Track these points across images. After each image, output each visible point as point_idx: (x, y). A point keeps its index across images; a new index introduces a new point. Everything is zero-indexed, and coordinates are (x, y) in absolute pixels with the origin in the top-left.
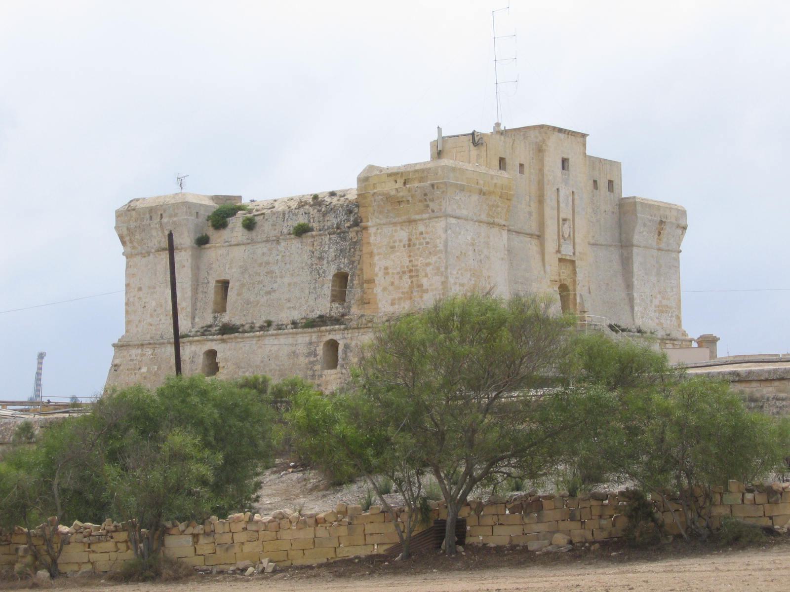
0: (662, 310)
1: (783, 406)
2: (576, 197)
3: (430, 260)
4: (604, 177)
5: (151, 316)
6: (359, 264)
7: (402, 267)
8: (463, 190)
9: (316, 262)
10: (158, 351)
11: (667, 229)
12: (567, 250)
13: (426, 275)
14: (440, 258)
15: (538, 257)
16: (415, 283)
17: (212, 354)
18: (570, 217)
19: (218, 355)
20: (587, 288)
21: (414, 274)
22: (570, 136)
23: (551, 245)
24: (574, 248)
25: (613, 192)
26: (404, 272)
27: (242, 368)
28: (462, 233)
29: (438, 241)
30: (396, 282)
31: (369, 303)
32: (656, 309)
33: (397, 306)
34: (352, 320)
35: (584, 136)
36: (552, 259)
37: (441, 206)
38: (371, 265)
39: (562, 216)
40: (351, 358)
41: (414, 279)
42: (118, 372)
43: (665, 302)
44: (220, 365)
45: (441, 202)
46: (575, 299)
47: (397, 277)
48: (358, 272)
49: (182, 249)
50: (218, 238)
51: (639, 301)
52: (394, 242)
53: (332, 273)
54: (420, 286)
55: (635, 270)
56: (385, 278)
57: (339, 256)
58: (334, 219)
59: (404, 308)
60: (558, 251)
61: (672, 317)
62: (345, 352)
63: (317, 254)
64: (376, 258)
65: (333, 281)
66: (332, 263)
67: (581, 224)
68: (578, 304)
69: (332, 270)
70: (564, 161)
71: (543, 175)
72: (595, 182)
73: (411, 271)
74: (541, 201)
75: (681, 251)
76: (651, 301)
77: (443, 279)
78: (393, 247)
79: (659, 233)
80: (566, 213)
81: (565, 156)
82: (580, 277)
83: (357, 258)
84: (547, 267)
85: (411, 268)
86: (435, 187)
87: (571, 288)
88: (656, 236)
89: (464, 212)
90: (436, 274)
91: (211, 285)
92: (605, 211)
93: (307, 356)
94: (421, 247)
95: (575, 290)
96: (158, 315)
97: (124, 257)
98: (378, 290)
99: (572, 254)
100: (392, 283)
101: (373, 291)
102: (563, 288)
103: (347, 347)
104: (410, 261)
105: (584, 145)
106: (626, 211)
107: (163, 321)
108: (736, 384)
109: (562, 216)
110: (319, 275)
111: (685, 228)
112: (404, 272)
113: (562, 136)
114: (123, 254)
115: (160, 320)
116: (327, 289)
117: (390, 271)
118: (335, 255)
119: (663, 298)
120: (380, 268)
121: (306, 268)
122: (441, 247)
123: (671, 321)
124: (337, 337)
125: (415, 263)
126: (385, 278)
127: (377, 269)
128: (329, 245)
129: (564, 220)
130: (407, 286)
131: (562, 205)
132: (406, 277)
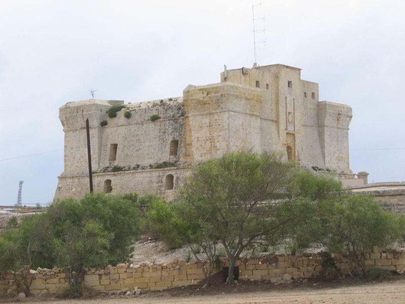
4: (310, 91)
10: (81, 180)
11: (342, 118)
12: (291, 128)
13: (218, 141)
18: (292, 111)
23: (282, 126)
26: (207, 140)
30: (203, 145)
31: (189, 156)
33: (203, 157)
35: (299, 70)
36: (283, 133)
38: (191, 136)
39: (288, 111)
43: (341, 155)
44: (113, 187)
50: (112, 122)
52: (202, 124)
60: (286, 129)
61: (344, 163)
62: (177, 181)
63: (162, 130)
64: (193, 133)
65: (171, 144)
67: (298, 115)
69: (170, 139)
70: (289, 83)
72: (305, 93)
73: (211, 139)
74: (277, 103)
76: (334, 155)
77: (227, 143)
78: (201, 127)
80: (290, 109)
82: (297, 142)
84: (280, 136)
88: (336, 121)
89: (238, 109)
95: (295, 149)
98: (194, 149)
102: (289, 148)
103: (178, 178)
105: (300, 74)
106: (321, 108)
109: (288, 111)
111: (351, 117)
112: (207, 140)
113: (288, 70)
116: (168, 149)
117: (200, 139)
122: (226, 127)
124: (172, 173)
129: (289, 113)
130: (209, 147)
131: (288, 105)
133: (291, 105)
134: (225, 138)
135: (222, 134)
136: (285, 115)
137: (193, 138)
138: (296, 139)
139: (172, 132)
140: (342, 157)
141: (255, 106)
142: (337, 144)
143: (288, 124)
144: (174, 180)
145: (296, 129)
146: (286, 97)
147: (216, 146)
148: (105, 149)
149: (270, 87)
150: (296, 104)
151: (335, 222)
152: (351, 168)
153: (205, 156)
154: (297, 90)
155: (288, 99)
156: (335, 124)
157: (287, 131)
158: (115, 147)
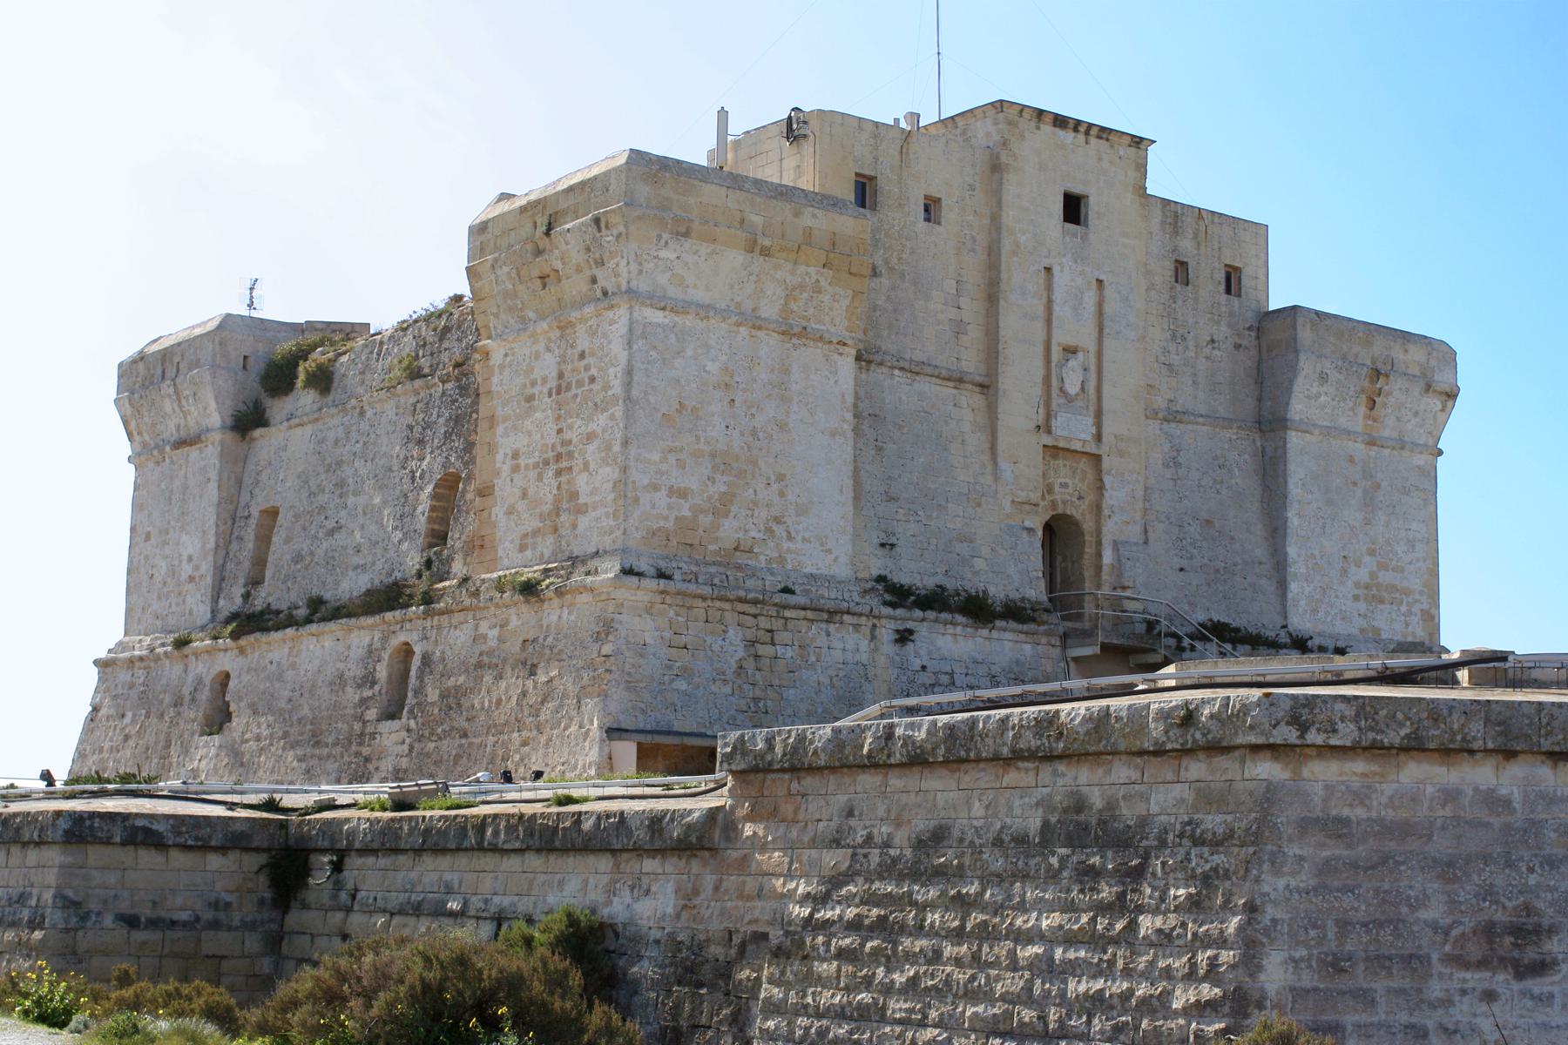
0: (1374, 594)
1: (1215, 869)
2: (1109, 292)
4: (1210, 258)
5: (159, 598)
8: (686, 234)
11: (1395, 389)
12: (1074, 428)
15: (976, 440)
16: (564, 486)
18: (1087, 340)
22: (1093, 140)
24: (1099, 424)
25: (1239, 295)
26: (546, 463)
28: (689, 353)
32: (1356, 592)
35: (1138, 142)
38: (492, 448)
39: (1060, 337)
40: (429, 689)
43: (1386, 577)
46: (1099, 555)
47: (533, 474)
50: (278, 409)
51: (1303, 570)
52: (533, 384)
54: (574, 495)
60: (1045, 427)
61: (1410, 613)
64: (500, 430)
66: (437, 452)
68: (1105, 570)
70: (1073, 208)
71: (999, 229)
73: (559, 457)
74: (992, 296)
75: (1440, 453)
76: (1344, 572)
78: (530, 399)
79: (1372, 404)
80: (1074, 328)
81: (1077, 190)
82: (1115, 495)
84: (1003, 464)
85: (559, 449)
86: (603, 225)
87: (1088, 525)
92: (1213, 341)
95: (1099, 532)
99: (1088, 437)
103: (426, 660)
104: (560, 431)
105: (1142, 168)
106: (1276, 339)
107: (174, 609)
108: (1061, 767)
111: (1451, 395)
112: (546, 463)
113: (1067, 136)
119: (1383, 566)
120: (506, 455)
122: (617, 387)
123: (1407, 625)
125: (568, 435)
129: (1071, 351)
130: (550, 498)
134: (608, 448)
136: (1039, 363)
137: (499, 457)
138: (1107, 479)
140: (1392, 588)
142: (1367, 522)
143: (1057, 400)
144: (413, 673)
145: (1107, 430)
146: (1048, 269)
149: (949, 214)
150: (1109, 309)
154: (1121, 247)
156: (1353, 418)
157: (1049, 441)
158: (272, 514)
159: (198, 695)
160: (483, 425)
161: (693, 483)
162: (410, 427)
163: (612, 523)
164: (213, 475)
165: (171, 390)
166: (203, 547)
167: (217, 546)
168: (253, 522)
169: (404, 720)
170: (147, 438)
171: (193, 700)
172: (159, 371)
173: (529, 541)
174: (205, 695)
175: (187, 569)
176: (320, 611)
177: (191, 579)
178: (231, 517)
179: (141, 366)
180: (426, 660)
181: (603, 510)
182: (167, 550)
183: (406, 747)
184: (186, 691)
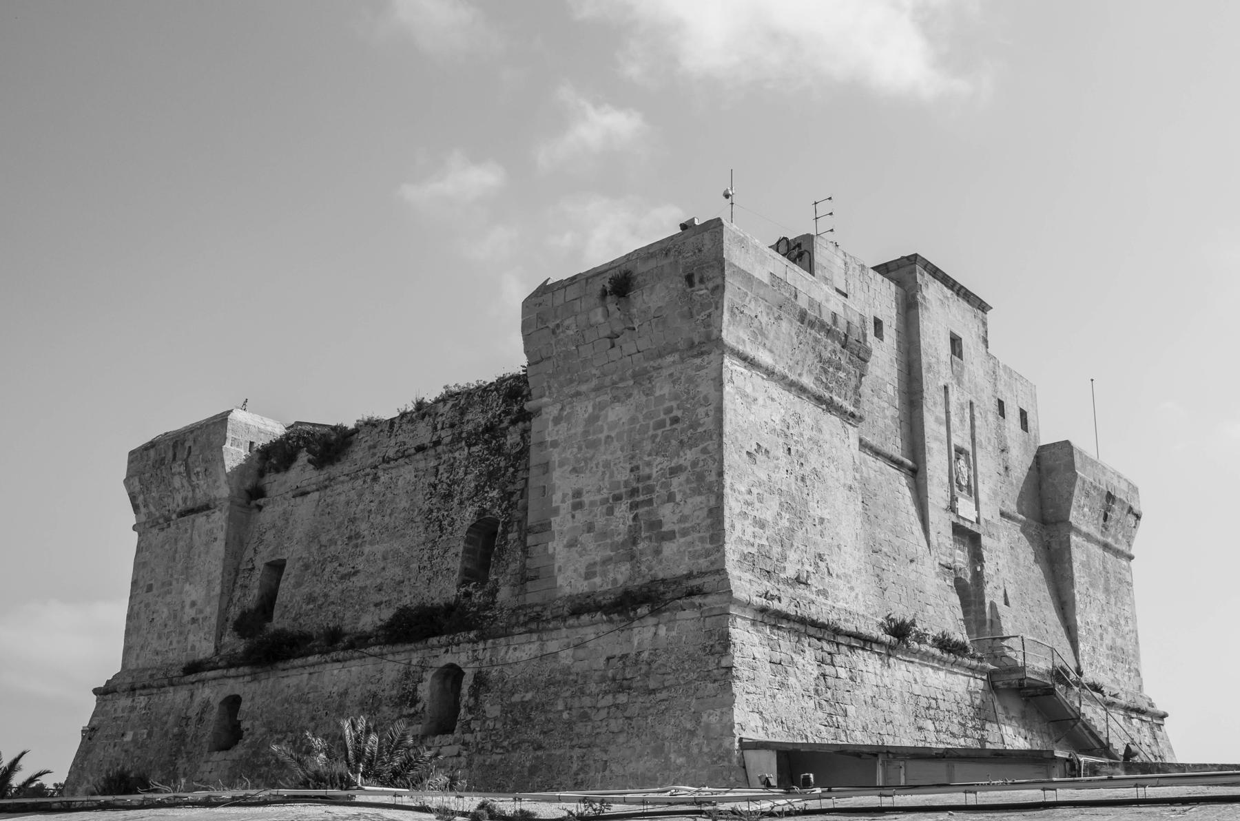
3: (681, 461)
5: (160, 637)
6: (521, 497)
7: (615, 485)
9: (438, 505)
10: (155, 699)
11: (1117, 512)
12: (966, 508)
13: (671, 498)
14: (704, 451)
17: (233, 703)
19: (244, 706)
20: (1001, 593)
21: (641, 498)
23: (937, 493)
26: (617, 498)
27: (276, 732)
29: (701, 411)
30: (600, 522)
31: (536, 578)
33: (597, 580)
34: (496, 619)
36: (940, 521)
37: (709, 326)
38: (544, 491)
40: (487, 706)
41: (642, 510)
42: (94, 741)
44: (245, 725)
45: (709, 316)
47: (600, 510)
48: (518, 514)
49: (216, 507)
53: (467, 524)
55: (1076, 575)
56: (573, 517)
57: (483, 487)
58: (481, 416)
59: (615, 581)
62: (475, 693)
63: (442, 489)
64: (556, 474)
65: (468, 541)
67: (987, 464)
69: (469, 514)
72: (1001, 404)
73: (634, 492)
77: (712, 502)
80: (961, 438)
83: (519, 485)
85: (635, 485)
86: (696, 279)
88: (1101, 519)
89: (765, 358)
90: (697, 492)
91: (257, 571)
93: (396, 705)
94: (659, 432)
96: (168, 635)
97: (136, 534)
98: (557, 546)
100: (590, 528)
101: (546, 549)
103: (481, 681)
107: (175, 645)
109: (956, 440)
110: (441, 530)
114: (134, 528)
115: (171, 643)
117: (586, 499)
118: (476, 486)
120: (565, 496)
121: (418, 519)
124: (461, 657)
125: (645, 471)
126: (573, 517)
127: (556, 498)
128: (467, 467)
130: (623, 528)
131: (954, 420)
132: (622, 509)
133: (962, 421)
135: (687, 464)
139: (479, 489)
141: (838, 368)
144: (465, 689)
147: (660, 524)
148: (247, 582)
151: (525, 709)
152: (1147, 692)
153: (604, 574)
155: (953, 398)
158: (277, 568)
159: (206, 716)
160: (534, 472)
161: (768, 516)
162: (434, 486)
163: (708, 546)
164: (221, 535)
165: (182, 469)
166: (208, 594)
167: (222, 593)
168: (257, 574)
169: (457, 734)
170: (152, 508)
171: (201, 720)
172: (170, 454)
173: (598, 568)
174: (213, 716)
175: (190, 612)
176: (336, 641)
177: (194, 620)
178: (235, 571)
179: (152, 452)
180: (481, 681)
181: (696, 535)
182: (168, 599)
183: (463, 760)
184: (192, 713)
